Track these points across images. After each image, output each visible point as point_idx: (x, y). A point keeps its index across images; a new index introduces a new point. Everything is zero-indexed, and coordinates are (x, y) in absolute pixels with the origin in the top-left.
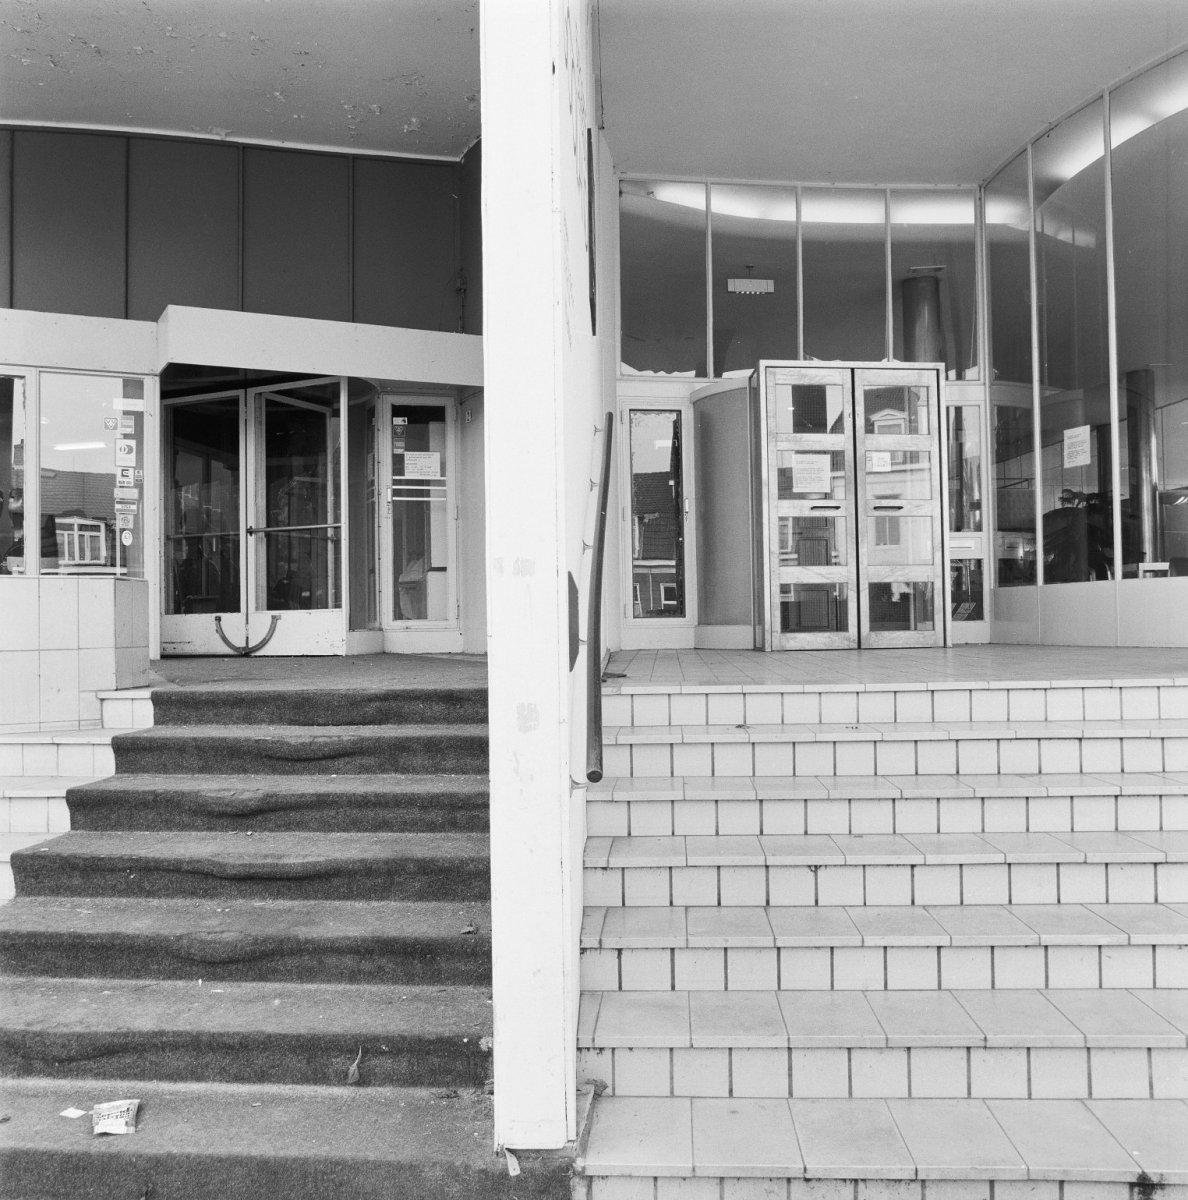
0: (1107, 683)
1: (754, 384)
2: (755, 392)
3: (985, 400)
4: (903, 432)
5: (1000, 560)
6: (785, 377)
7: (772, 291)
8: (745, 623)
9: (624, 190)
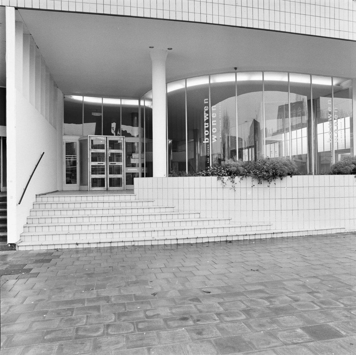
0: (112, 195)
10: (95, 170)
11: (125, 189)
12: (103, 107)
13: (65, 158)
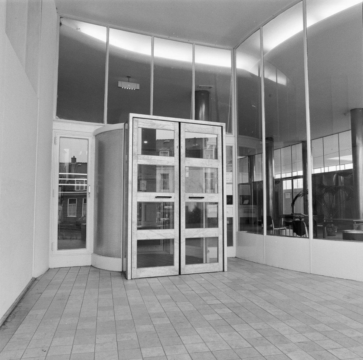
1: (126, 128)
2: (127, 131)
3: (235, 144)
4: (169, 155)
5: (240, 218)
6: (143, 124)
7: (139, 89)
8: (119, 257)
9: (63, 23)
10: (151, 215)
11: (226, 269)
12: (155, 66)
13: (57, 179)
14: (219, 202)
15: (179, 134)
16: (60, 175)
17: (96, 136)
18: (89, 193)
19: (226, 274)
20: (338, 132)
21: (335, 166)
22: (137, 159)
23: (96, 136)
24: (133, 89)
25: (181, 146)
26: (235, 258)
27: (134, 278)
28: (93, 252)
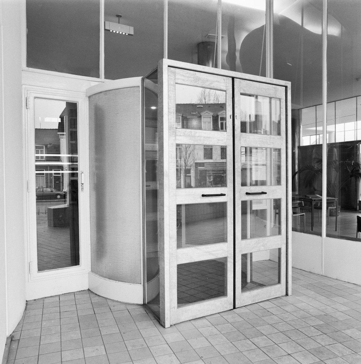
11: (290, 293)
14: (282, 198)
15: (232, 97)
16: (37, 157)
17: (89, 97)
18: (83, 184)
19: (289, 299)
20: (335, 100)
21: (309, 136)
22: (175, 136)
23: (89, 97)
24: (125, 34)
25: (235, 115)
26: (269, 261)
27: (175, 323)
28: (90, 270)
